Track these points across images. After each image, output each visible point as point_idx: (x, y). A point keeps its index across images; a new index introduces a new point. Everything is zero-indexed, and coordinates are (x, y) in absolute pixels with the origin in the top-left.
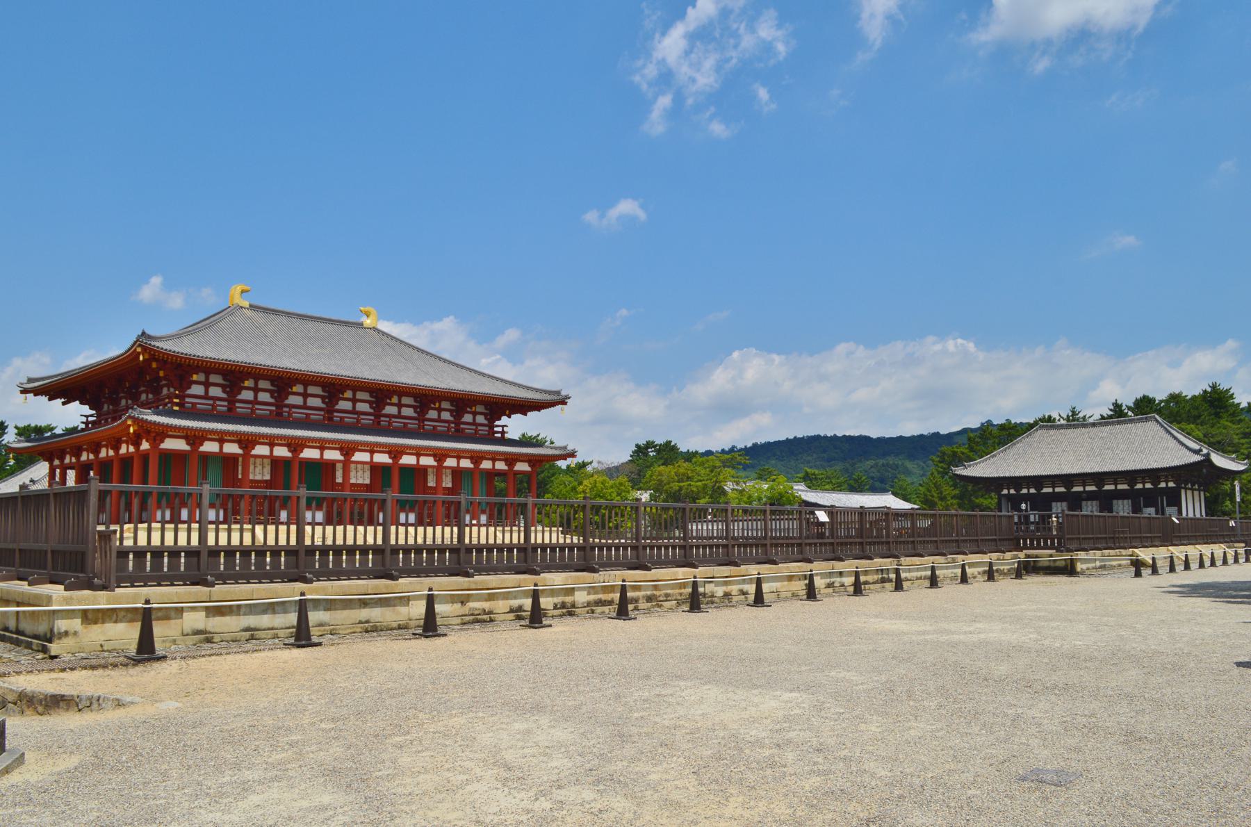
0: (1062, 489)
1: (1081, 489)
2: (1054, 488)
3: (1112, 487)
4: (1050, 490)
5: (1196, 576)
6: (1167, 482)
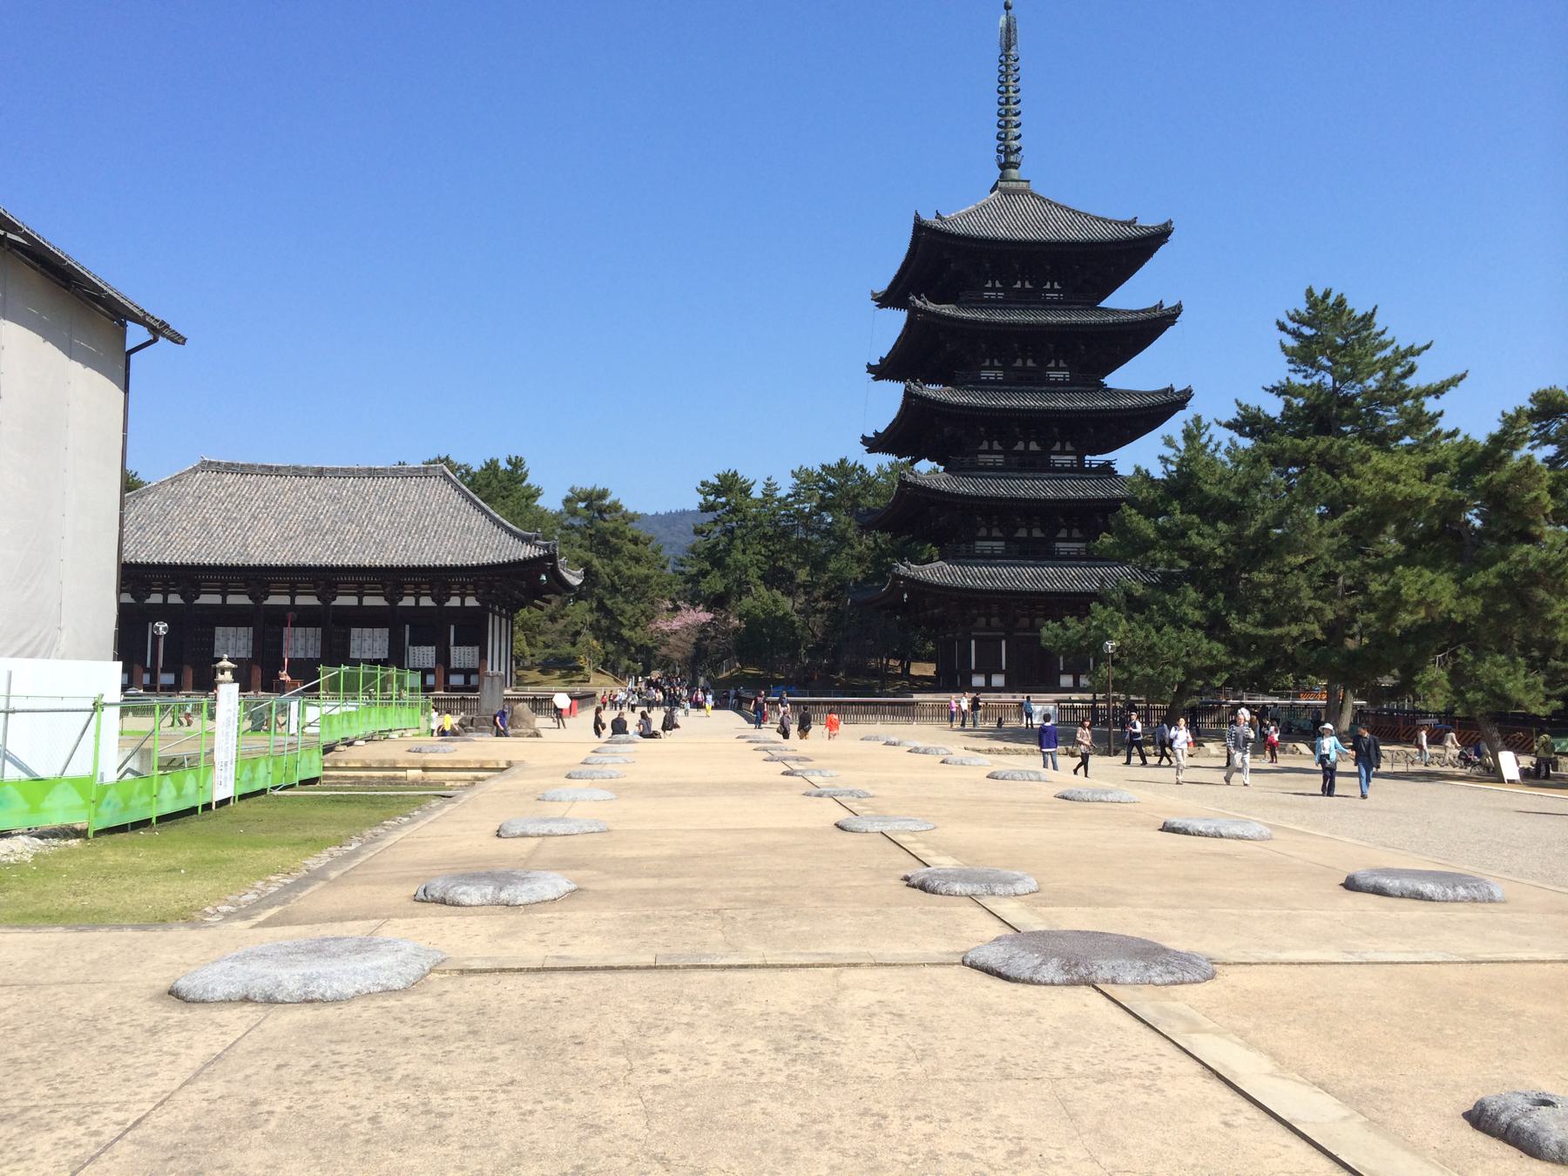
0: (244, 600)
1: (284, 600)
2: (360, 595)
3: (352, 601)
4: (216, 599)
5: (261, 918)
6: (417, 596)
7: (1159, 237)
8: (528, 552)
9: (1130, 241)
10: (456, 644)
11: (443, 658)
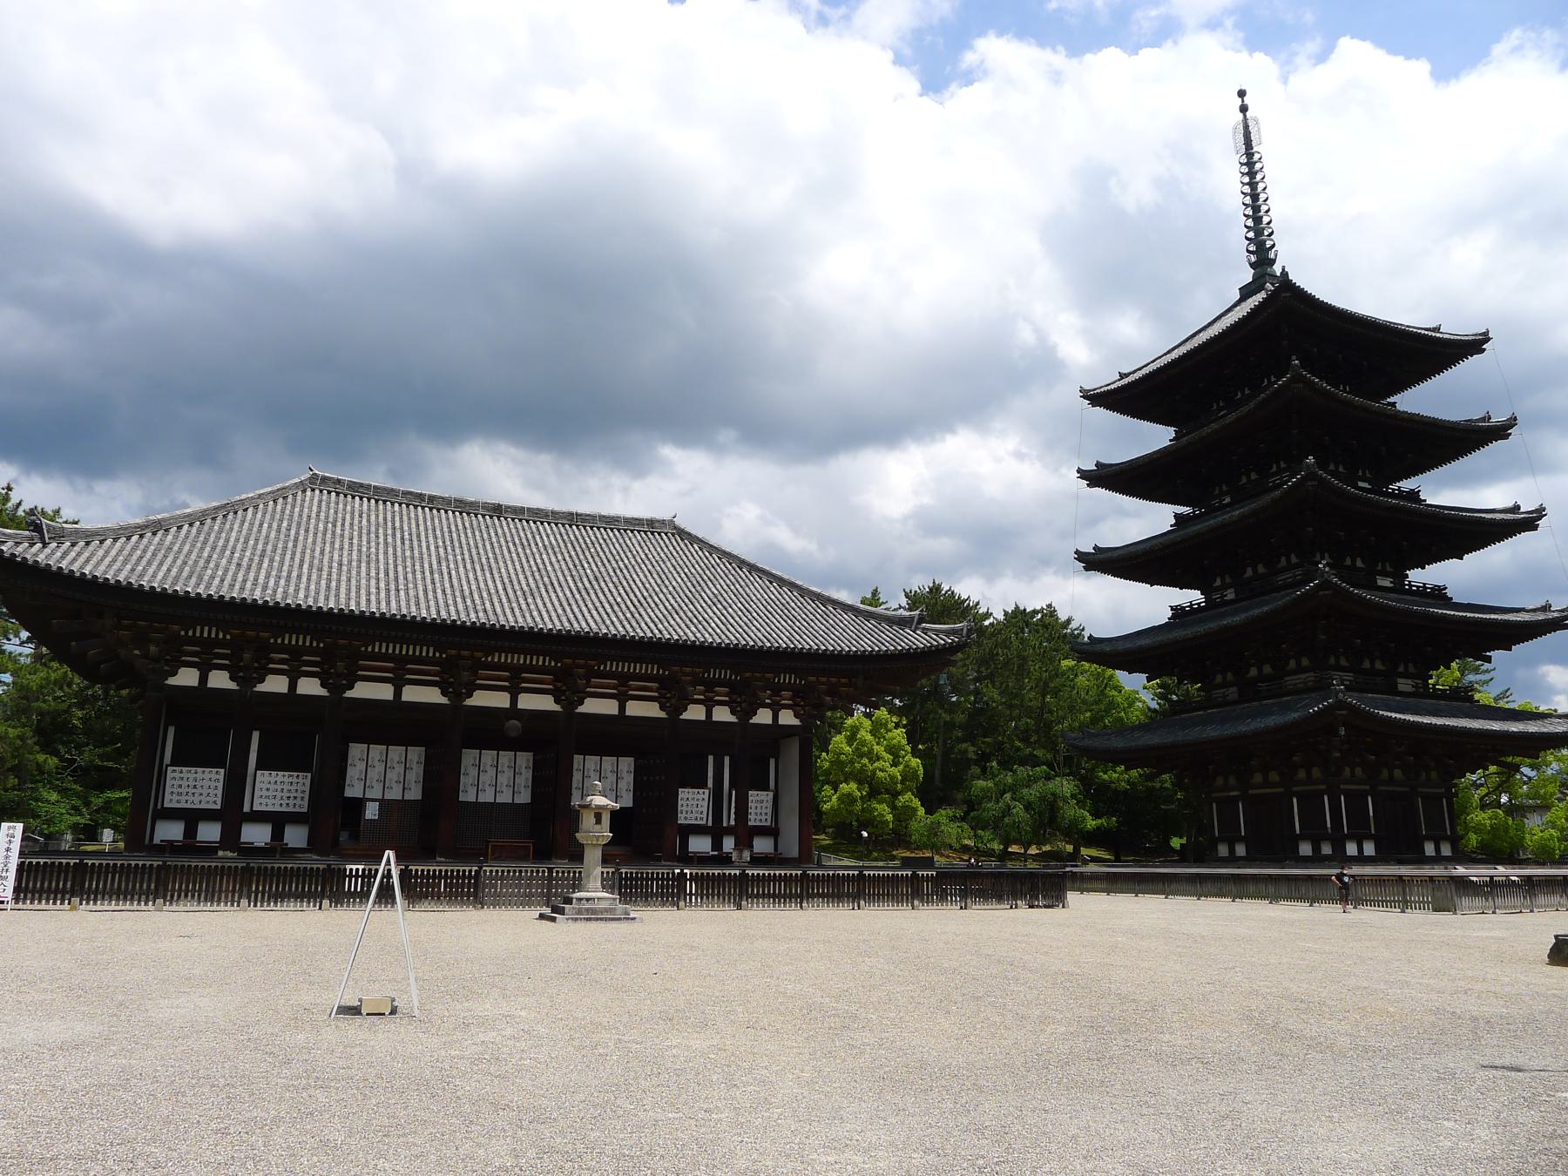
1: (500, 700)
2: (622, 700)
6: (709, 705)
10: (176, 762)
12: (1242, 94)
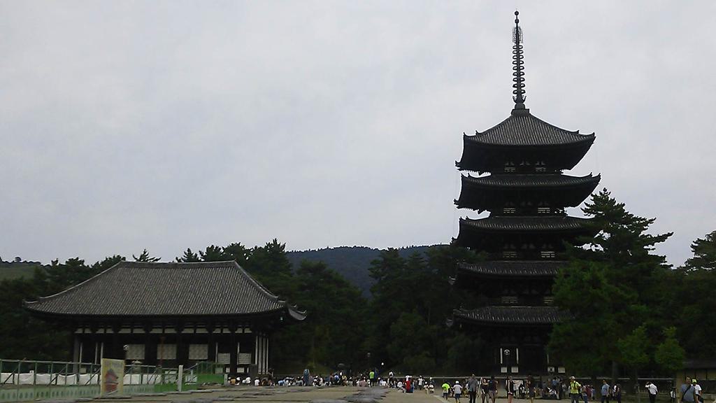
3: (191, 331)
7: (590, 139)
8: (274, 306)
9: (578, 143)
11: (234, 358)
12: (517, 13)
